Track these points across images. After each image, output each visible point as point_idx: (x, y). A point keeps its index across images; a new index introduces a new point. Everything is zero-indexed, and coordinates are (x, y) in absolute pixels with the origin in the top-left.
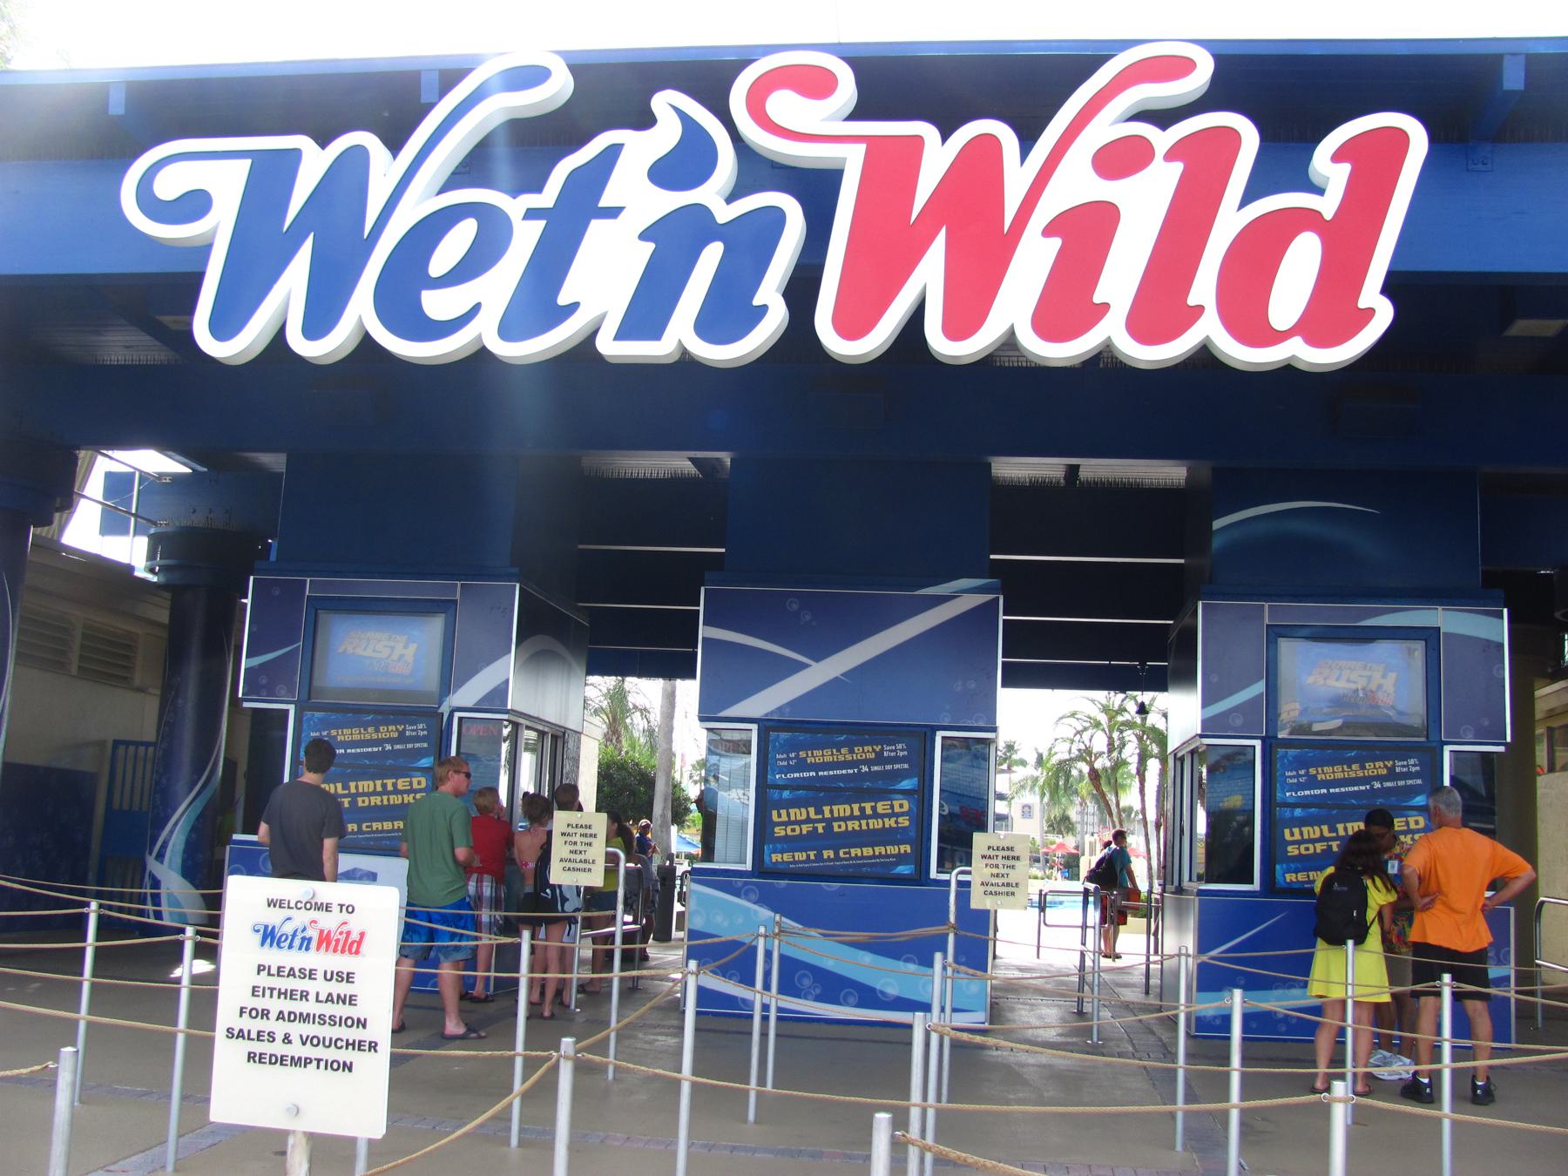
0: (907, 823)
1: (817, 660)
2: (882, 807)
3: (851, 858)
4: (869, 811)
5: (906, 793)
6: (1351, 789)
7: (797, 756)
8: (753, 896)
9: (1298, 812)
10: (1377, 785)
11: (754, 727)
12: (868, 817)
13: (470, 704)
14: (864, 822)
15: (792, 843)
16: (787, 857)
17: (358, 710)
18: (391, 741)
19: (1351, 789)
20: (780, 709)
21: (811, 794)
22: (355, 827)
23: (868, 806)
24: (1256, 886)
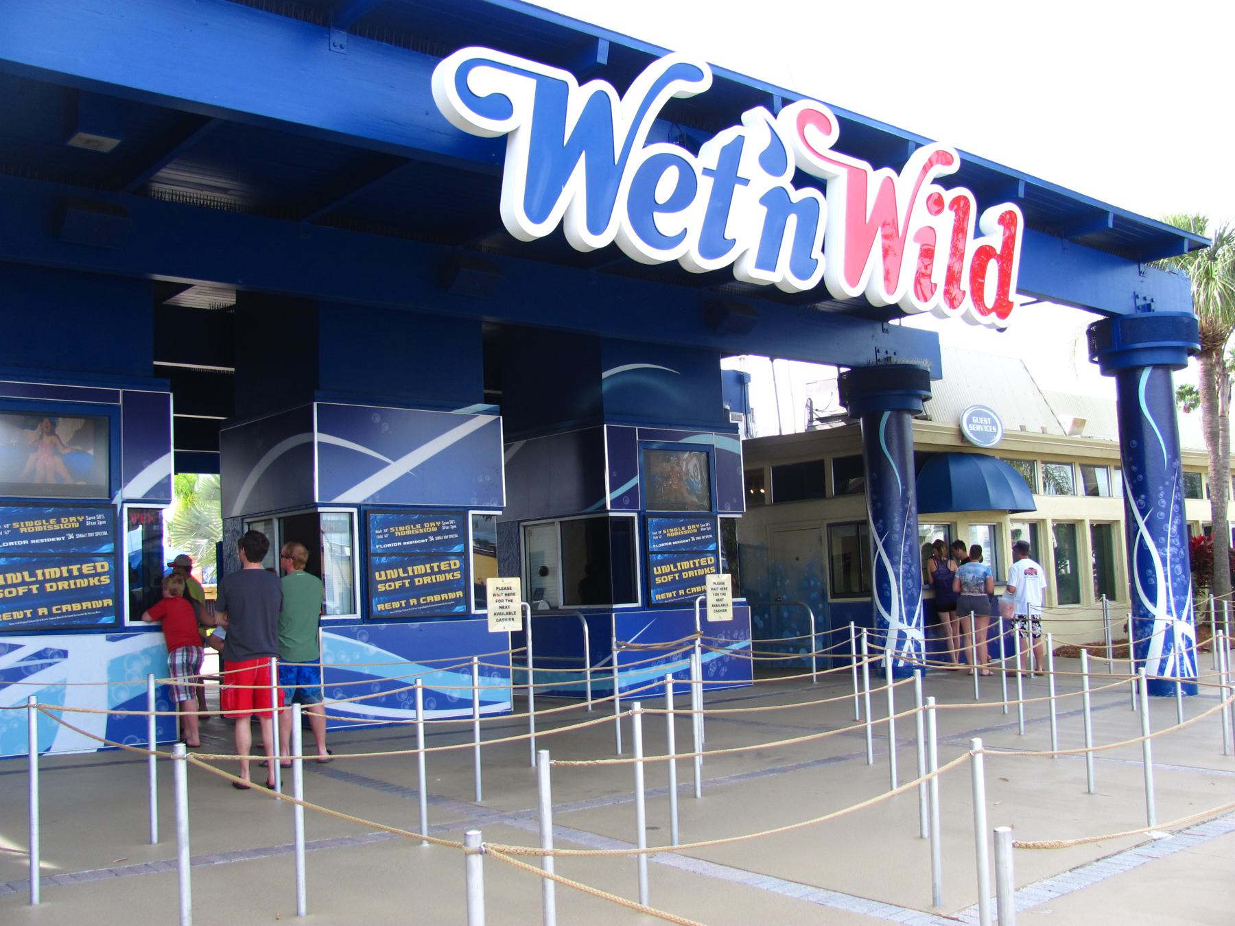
0: (108, 581)
1: (395, 460)
2: (86, 569)
3: (63, 614)
4: (76, 573)
5: (106, 556)
6: (49, 540)
7: (11, 528)
8: (365, 638)
9: (659, 557)
10: (71, 536)
11: (355, 510)
12: (75, 578)
13: (139, 496)
14: (72, 582)
15: (390, 596)
16: (388, 606)
17: (38, 503)
18: (434, 534)
19: (49, 540)
20: (372, 496)
21: (399, 558)
22: (45, 611)
23: (75, 568)
24: (639, 604)
